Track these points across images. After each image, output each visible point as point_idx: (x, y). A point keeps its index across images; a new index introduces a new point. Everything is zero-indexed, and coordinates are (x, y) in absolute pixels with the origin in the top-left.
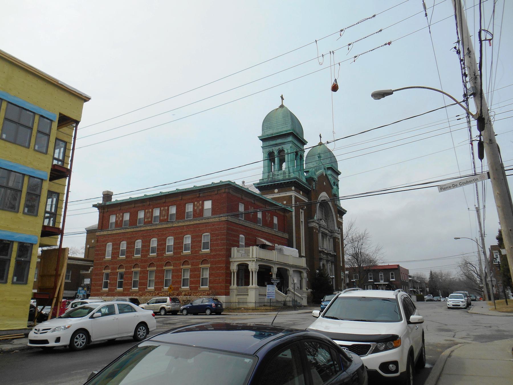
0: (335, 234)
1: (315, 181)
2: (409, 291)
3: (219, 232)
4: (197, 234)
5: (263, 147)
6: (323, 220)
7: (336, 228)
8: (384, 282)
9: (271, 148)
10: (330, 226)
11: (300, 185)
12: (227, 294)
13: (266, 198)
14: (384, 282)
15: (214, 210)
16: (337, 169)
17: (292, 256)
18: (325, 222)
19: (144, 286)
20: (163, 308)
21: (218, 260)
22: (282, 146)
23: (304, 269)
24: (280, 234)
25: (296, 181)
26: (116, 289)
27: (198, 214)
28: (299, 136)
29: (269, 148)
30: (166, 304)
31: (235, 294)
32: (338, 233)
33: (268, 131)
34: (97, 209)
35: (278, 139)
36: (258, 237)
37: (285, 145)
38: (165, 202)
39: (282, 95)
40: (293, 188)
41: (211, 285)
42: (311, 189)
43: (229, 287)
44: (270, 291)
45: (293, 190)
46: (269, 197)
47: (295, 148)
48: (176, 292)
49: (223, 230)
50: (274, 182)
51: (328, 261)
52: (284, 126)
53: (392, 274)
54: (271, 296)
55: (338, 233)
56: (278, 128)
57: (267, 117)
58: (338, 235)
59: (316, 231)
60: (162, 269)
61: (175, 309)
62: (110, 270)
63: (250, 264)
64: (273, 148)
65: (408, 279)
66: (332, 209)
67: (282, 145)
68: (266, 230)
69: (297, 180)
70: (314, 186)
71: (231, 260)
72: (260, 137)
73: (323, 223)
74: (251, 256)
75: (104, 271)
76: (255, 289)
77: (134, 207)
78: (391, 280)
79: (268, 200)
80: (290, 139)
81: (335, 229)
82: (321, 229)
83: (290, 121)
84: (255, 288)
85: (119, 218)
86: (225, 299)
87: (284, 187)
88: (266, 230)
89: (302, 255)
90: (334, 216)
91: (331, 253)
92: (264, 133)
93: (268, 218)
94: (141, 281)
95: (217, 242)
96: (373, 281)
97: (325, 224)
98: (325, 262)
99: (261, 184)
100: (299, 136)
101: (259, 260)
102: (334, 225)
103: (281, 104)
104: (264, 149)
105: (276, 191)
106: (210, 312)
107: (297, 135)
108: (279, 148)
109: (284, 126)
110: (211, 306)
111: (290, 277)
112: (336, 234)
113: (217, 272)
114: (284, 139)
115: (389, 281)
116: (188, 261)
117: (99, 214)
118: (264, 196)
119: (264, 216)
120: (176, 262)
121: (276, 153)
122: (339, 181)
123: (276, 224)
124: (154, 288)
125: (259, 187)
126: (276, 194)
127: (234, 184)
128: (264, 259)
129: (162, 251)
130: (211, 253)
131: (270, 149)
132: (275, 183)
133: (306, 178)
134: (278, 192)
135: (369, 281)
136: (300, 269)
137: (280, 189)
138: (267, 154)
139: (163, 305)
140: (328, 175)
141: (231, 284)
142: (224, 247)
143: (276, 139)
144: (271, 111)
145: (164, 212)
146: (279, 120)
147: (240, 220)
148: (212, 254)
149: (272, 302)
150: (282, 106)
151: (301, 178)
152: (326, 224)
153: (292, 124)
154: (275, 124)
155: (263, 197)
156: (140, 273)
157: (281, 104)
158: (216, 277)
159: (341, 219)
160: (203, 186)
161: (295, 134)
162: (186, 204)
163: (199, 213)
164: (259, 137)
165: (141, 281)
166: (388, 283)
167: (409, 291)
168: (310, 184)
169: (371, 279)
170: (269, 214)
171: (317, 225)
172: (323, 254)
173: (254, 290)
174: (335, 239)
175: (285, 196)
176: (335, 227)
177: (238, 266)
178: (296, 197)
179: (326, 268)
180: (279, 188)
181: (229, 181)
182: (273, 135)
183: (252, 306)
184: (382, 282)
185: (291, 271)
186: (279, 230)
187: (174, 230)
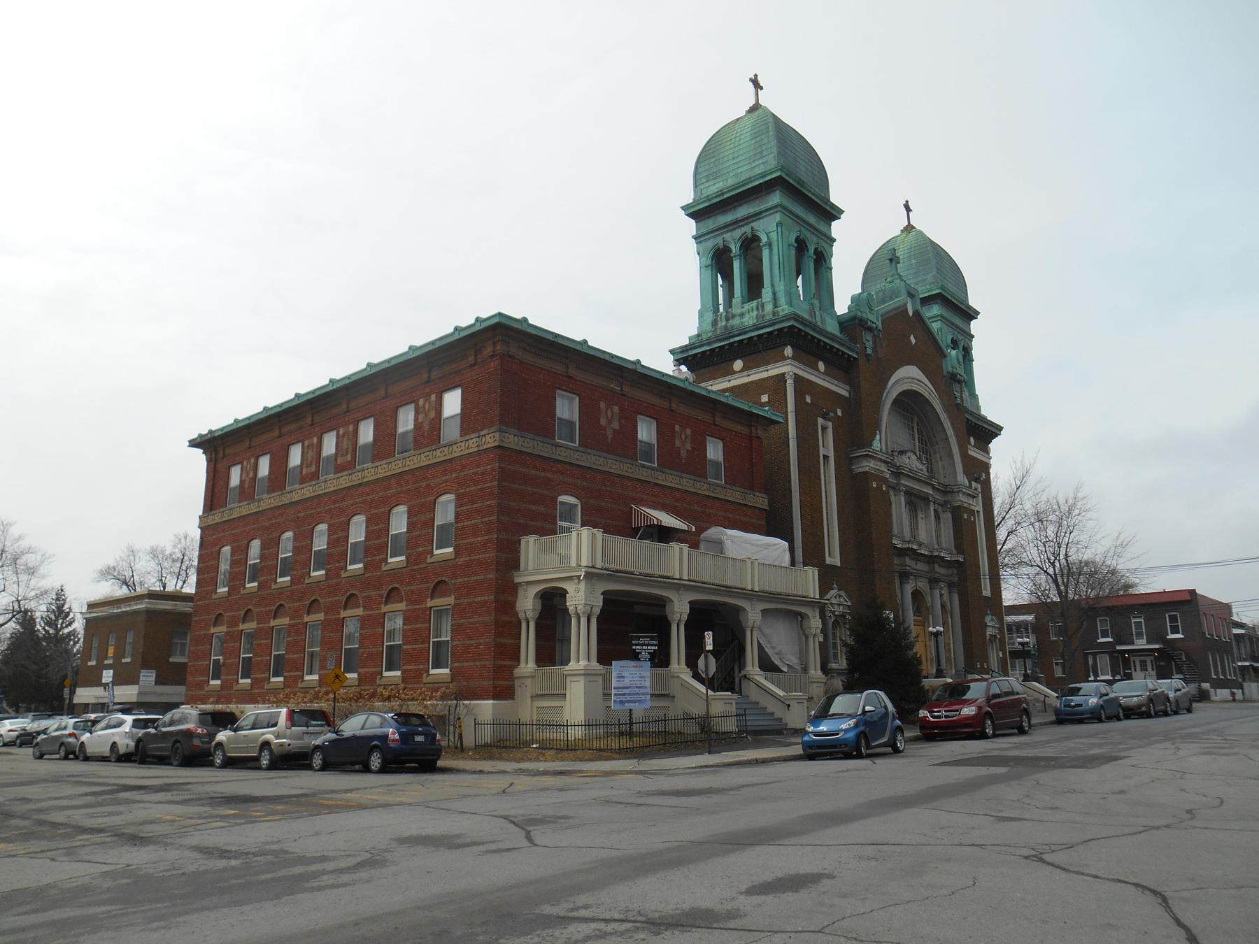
0: (957, 498)
1: (870, 329)
2: (1234, 668)
3: (479, 487)
4: (423, 500)
6: (910, 454)
7: (962, 479)
8: (1149, 642)
9: (721, 237)
11: (988, 433)
12: (504, 691)
13: (709, 391)
14: (1149, 642)
15: (468, 420)
16: (827, 200)
17: (756, 563)
18: (919, 459)
19: (295, 671)
20: (266, 744)
21: (476, 581)
22: (752, 224)
23: (811, 604)
24: (734, 495)
25: (792, 326)
26: (238, 681)
27: (426, 434)
28: (810, 191)
29: (714, 237)
30: (274, 731)
31: (529, 695)
32: (969, 495)
33: (709, 186)
34: (202, 451)
35: (741, 205)
36: (641, 502)
37: (761, 221)
38: (347, 411)
39: (756, 76)
40: (788, 351)
41: (456, 665)
42: (857, 353)
43: (512, 668)
44: (626, 682)
45: (788, 358)
46: (716, 386)
47: (951, 330)
48: (369, 690)
49: (491, 481)
50: (730, 337)
51: (933, 581)
52: (757, 163)
53: (1173, 619)
54: (634, 702)
55: (969, 495)
56: (739, 170)
57: (871, 263)
58: (971, 500)
59: (879, 488)
60: (337, 616)
61: (303, 747)
62: (255, 622)
63: (570, 587)
64: (728, 236)
65: (1229, 631)
66: (943, 419)
67: (753, 221)
68: (670, 479)
69: (796, 325)
70: (869, 345)
71: (517, 580)
72: (688, 208)
73: (912, 462)
75: (213, 630)
76: (584, 675)
77: (280, 436)
78: (1171, 636)
79: (713, 396)
80: (776, 198)
83: (773, 143)
84: (583, 672)
85: (248, 474)
86: (491, 713)
87: (760, 351)
88: (670, 479)
90: (951, 440)
91: (942, 555)
92: (699, 192)
93: (610, 421)
94: (291, 656)
95: (473, 522)
96: (1112, 640)
97: (920, 466)
98: (923, 585)
99: (692, 349)
100: (810, 191)
101: (603, 575)
102: (953, 464)
103: (752, 102)
104: (701, 242)
105: (738, 365)
106: (379, 761)
107: (799, 187)
108: (743, 232)
109: (757, 163)
110: (384, 738)
111: (748, 633)
112: (962, 497)
113: (471, 620)
114: (757, 202)
115: (1163, 639)
116: (400, 587)
117: (207, 465)
118: (703, 385)
119: (664, 433)
120: (371, 593)
121: (735, 249)
122: (973, 337)
123: (717, 464)
124: (399, 674)
125: (684, 356)
126: (740, 376)
127: (638, 365)
128: (632, 573)
129: (338, 561)
130: (457, 560)
131: (719, 241)
132: (732, 340)
133: (838, 323)
134: (745, 368)
135: (1098, 641)
136: (792, 604)
138: (710, 256)
139: (268, 735)
140: (930, 318)
141: (518, 660)
142: (490, 537)
143: (735, 207)
144: (720, 128)
145: (345, 439)
146: (741, 147)
147: (557, 446)
148: (461, 560)
150: (909, 228)
151: (818, 319)
152: (924, 468)
153: (779, 153)
154: (731, 162)
155: (700, 387)
156: (289, 633)
157: (754, 103)
158: (470, 638)
159: (983, 453)
160: (433, 343)
161: (791, 181)
162: (398, 407)
163: (429, 432)
164: (683, 208)
165: (291, 656)
166: (1162, 646)
167: (1234, 668)
168: (854, 339)
169: (1105, 634)
170: (689, 432)
171: (883, 468)
172: (911, 559)
173: (582, 679)
174: (957, 512)
175: (764, 379)
176: (958, 475)
177: (541, 598)
178: (798, 379)
179: (929, 604)
180: (745, 356)
181: (500, 314)
182: (723, 194)
183: (580, 737)
184: (1141, 644)
185: (753, 614)
186: (731, 481)
187: (368, 494)
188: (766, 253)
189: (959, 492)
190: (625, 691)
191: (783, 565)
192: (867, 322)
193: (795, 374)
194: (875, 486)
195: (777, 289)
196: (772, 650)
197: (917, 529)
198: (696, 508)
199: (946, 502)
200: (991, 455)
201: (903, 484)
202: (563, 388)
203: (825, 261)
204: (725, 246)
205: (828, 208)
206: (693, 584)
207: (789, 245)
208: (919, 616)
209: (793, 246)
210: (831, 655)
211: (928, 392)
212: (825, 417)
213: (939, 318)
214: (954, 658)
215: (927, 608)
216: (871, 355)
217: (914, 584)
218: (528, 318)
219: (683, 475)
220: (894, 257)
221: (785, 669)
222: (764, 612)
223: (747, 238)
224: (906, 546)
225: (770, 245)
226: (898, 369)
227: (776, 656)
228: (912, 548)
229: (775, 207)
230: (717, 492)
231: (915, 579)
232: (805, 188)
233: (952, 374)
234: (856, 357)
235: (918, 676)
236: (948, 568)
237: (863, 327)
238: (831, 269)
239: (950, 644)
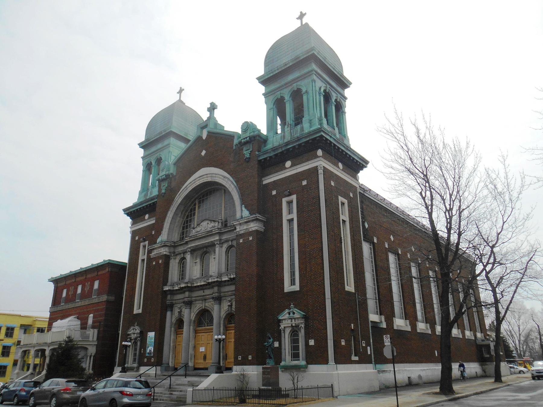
5: (265, 95)
40: (320, 152)
89: (346, 289)
105: (288, 164)
121: (287, 97)
131: (278, 95)
149: (284, 390)
164: (258, 79)
178: (325, 170)
188: (305, 97)
193: (324, 167)
204: (281, 97)
206: (522, 402)
219: (86, 299)
235: (305, 327)
238: (345, 113)
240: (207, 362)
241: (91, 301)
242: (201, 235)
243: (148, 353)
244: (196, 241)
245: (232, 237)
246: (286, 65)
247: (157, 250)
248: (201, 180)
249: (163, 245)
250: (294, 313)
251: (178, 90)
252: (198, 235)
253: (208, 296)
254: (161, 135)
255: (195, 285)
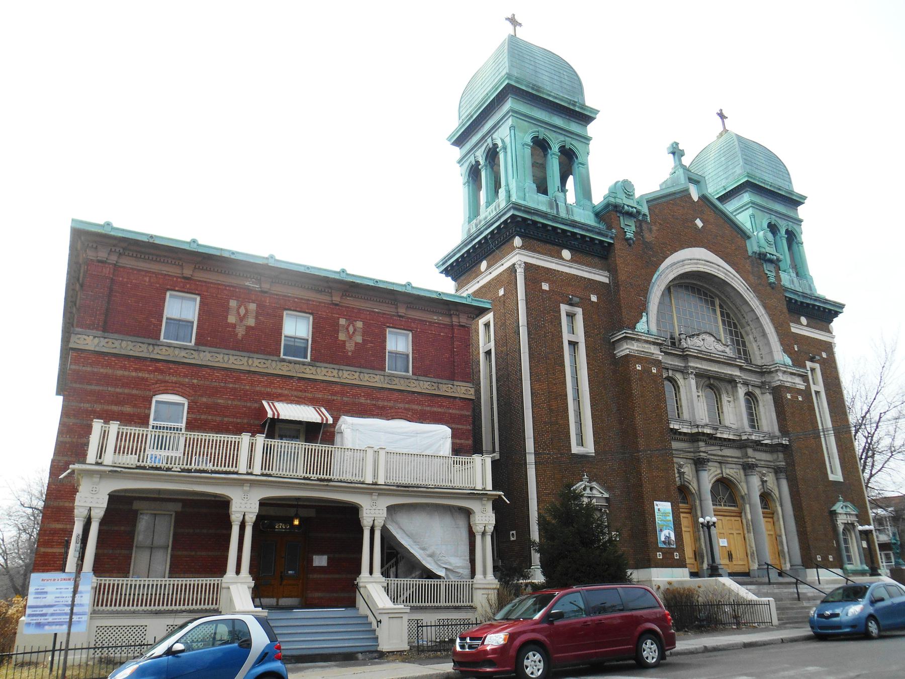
0: (776, 378)
10: (757, 353)
39: (721, 110)
40: (518, 241)
42: (611, 238)
51: (748, 468)
74: (91, 456)
81: (773, 360)
82: (691, 364)
87: (494, 251)
102: (768, 344)
105: (484, 265)
112: (781, 376)
122: (801, 221)
131: (472, 160)
134: (489, 267)
137: (490, 257)
161: (524, 88)
172: (755, 450)
178: (528, 267)
182: (472, 117)
189: (777, 371)
190: (45, 611)
191: (441, 454)
192: (623, 208)
194: (640, 368)
195: (511, 187)
196: (422, 552)
197: (722, 412)
198: (363, 401)
199: (763, 383)
200: (834, 334)
201: (690, 367)
202: (177, 289)
203: (796, 238)
205: (577, 109)
207: (523, 145)
208: (734, 506)
209: (557, 155)
210: (845, 559)
211: (724, 273)
212: (812, 360)
213: (750, 205)
214: (789, 552)
215: (743, 497)
216: (774, 283)
217: (719, 471)
218: (272, 253)
219: (342, 367)
220: (675, 150)
221: (442, 573)
222: (391, 509)
223: (490, 149)
224: (695, 430)
225: (505, 148)
226: (676, 251)
227: (429, 559)
228: (782, 444)
229: (508, 113)
230: (394, 383)
231: (721, 465)
232: (543, 93)
233: (760, 254)
234: (612, 242)
236: (771, 452)
237: (621, 212)
239: (780, 536)
240: (734, 562)
241: (330, 374)
242: (718, 358)
243: (664, 542)
244: (704, 362)
245: (755, 381)
246: (779, 189)
247: (640, 345)
248: (715, 270)
249: (660, 341)
250: (591, 489)
251: (518, 18)
252: (714, 355)
253: (730, 459)
254: (572, 107)
255: (719, 435)
